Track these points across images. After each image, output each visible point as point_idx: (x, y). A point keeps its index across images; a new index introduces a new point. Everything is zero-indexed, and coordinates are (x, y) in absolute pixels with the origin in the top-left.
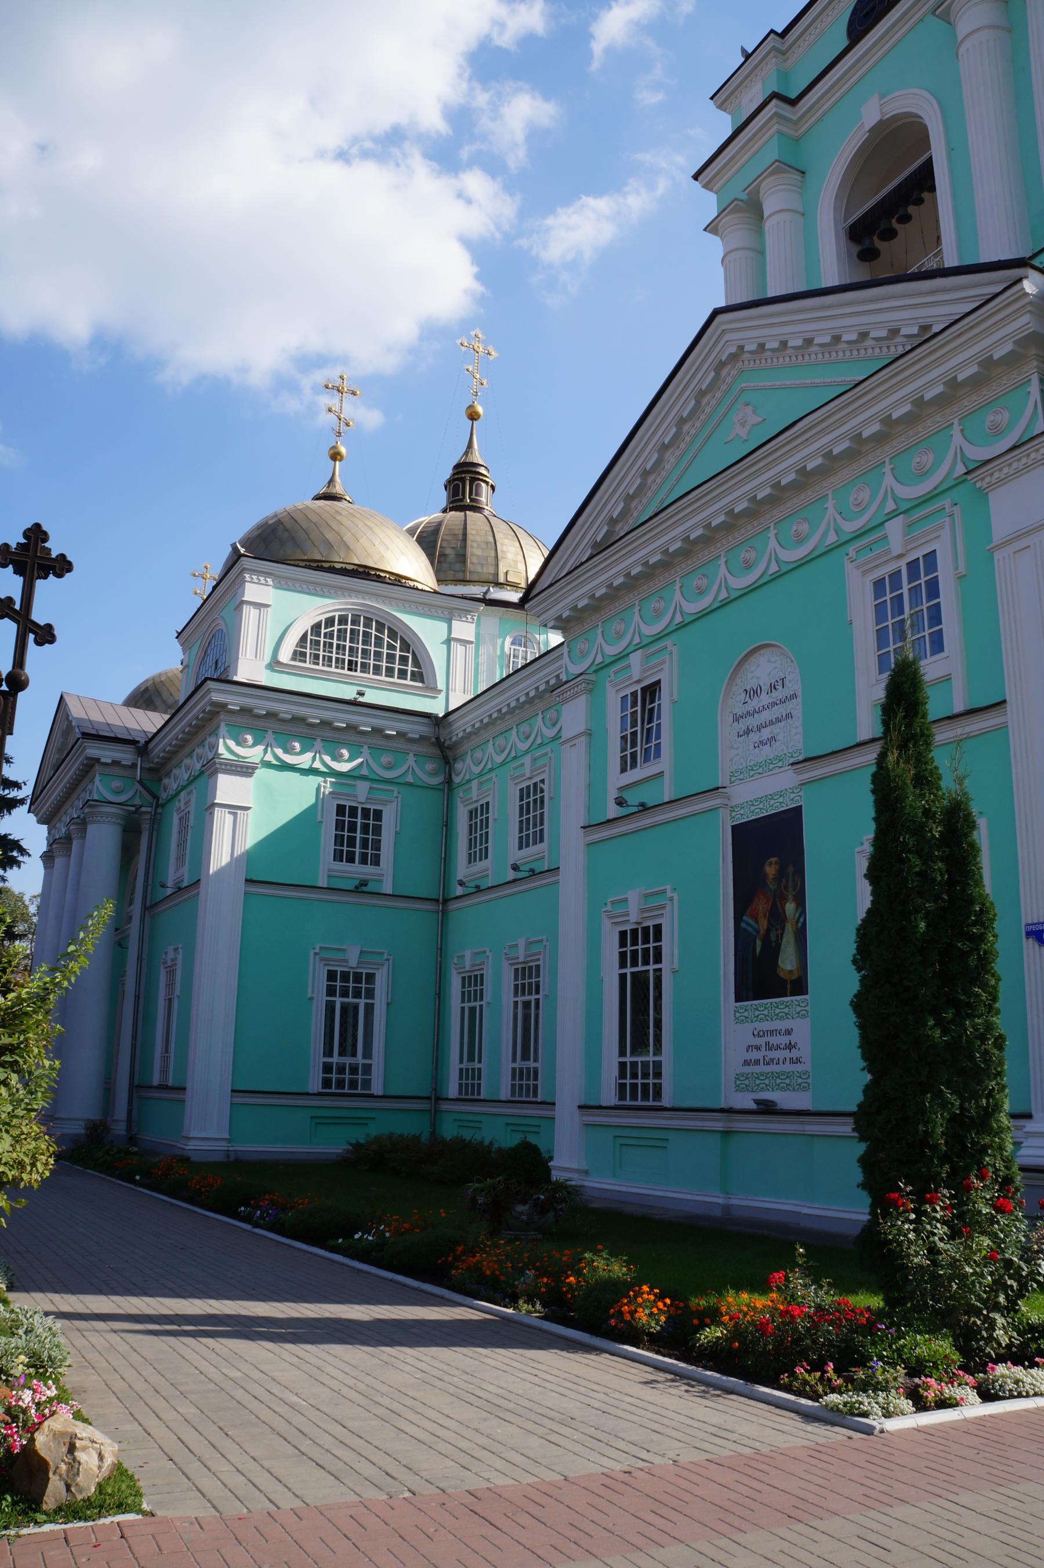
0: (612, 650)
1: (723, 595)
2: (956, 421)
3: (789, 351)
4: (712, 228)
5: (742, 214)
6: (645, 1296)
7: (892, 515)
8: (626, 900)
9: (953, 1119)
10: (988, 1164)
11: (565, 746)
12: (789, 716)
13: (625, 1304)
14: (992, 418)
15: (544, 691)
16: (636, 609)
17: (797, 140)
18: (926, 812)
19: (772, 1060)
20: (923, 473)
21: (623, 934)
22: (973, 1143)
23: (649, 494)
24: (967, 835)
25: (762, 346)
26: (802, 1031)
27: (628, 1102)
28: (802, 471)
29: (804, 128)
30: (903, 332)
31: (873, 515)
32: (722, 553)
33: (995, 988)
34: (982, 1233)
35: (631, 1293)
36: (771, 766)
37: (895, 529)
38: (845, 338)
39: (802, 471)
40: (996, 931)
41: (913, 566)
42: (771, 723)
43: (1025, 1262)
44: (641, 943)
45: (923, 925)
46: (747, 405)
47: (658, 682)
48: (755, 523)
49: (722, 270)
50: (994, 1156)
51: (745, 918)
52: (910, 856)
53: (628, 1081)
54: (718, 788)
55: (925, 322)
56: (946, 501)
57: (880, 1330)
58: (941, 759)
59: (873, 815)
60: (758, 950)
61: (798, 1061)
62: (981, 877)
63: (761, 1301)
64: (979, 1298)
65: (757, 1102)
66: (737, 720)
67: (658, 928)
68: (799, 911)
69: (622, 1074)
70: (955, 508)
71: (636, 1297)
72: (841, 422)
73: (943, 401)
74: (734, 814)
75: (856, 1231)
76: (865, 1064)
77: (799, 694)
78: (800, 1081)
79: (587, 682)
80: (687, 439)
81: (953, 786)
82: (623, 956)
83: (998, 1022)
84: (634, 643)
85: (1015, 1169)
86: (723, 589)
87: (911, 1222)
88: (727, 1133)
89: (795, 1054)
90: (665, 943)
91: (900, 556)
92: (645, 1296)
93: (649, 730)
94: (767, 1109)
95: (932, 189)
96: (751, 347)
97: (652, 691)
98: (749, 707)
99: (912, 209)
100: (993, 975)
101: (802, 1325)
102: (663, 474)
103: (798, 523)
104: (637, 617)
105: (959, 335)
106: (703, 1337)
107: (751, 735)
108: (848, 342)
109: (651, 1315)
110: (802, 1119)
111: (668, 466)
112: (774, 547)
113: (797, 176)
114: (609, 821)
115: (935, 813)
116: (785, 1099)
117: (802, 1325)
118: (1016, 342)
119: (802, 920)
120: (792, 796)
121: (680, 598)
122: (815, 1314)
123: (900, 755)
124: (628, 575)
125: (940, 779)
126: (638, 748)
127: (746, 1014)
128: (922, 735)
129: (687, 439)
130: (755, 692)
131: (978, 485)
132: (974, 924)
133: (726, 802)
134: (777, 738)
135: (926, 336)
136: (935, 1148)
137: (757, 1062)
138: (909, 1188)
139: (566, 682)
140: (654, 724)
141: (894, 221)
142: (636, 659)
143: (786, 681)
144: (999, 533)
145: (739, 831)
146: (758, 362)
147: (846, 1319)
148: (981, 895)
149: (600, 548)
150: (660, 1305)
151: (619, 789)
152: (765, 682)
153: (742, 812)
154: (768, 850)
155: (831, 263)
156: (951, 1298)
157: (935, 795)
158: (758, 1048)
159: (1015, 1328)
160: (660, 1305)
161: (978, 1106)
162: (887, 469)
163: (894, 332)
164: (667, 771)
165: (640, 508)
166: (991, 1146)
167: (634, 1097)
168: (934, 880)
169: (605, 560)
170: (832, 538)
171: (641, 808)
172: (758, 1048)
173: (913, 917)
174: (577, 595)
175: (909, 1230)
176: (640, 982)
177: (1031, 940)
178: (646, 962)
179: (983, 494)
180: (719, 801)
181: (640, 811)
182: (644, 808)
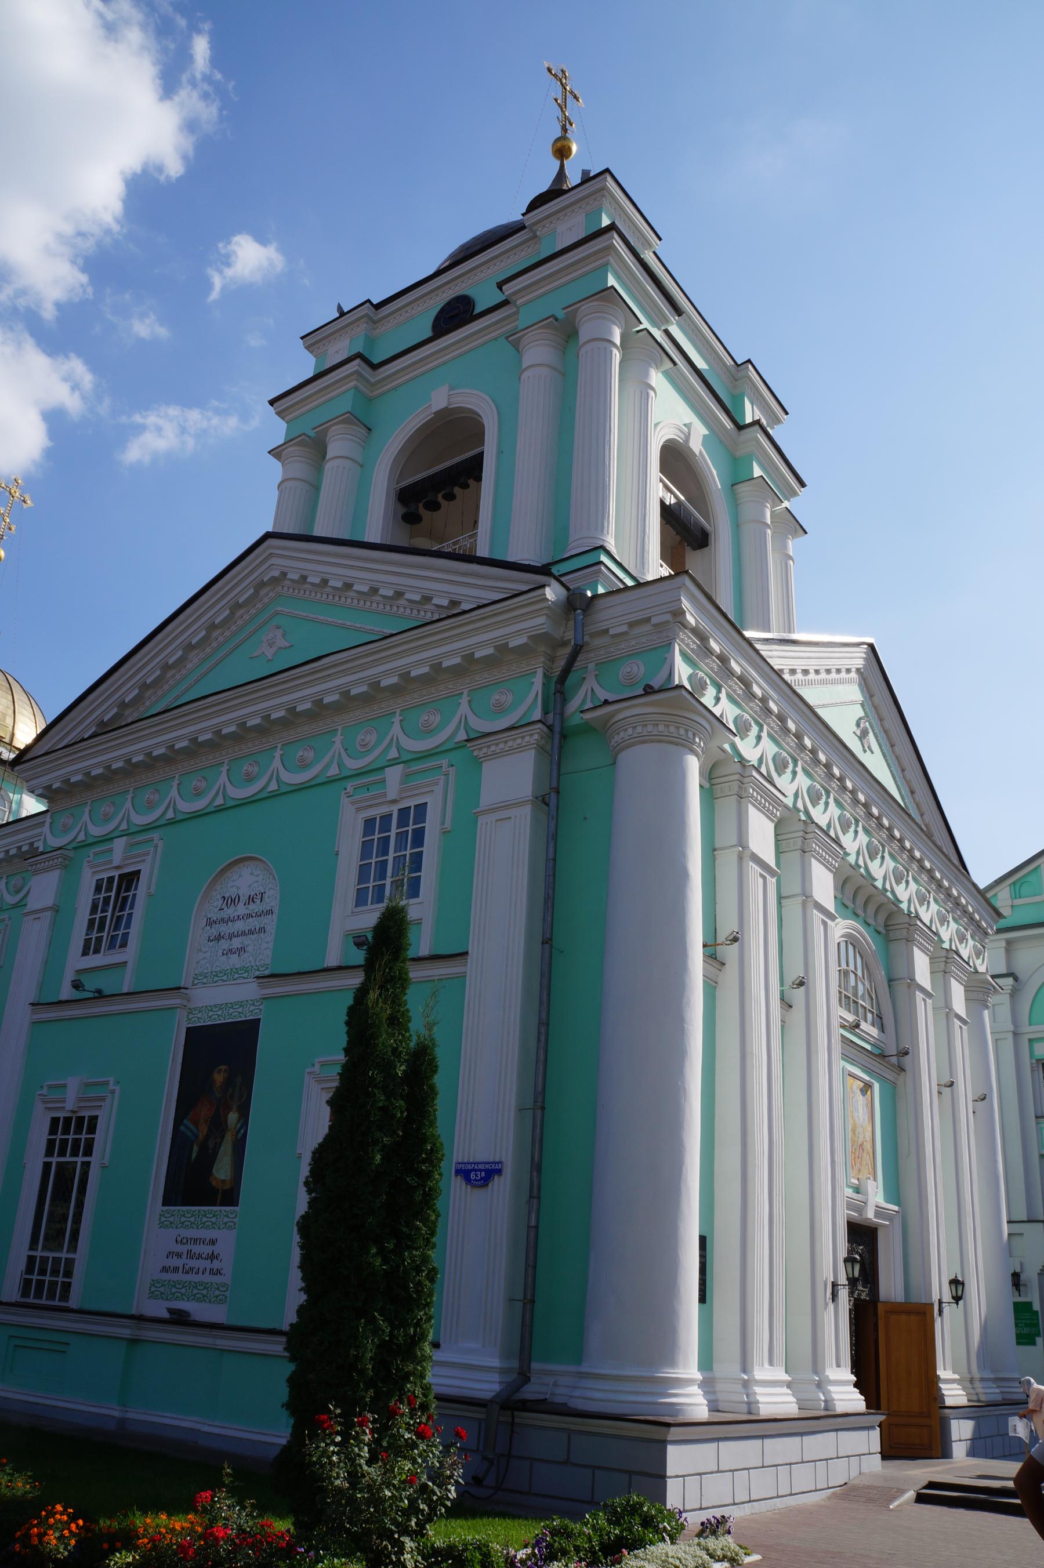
0: (96, 831)
1: (219, 801)
2: (466, 692)
3: (327, 590)
4: (276, 453)
5: (305, 450)
6: (58, 1516)
7: (394, 762)
8: (64, 1086)
9: (382, 1346)
10: (409, 1390)
11: (26, 918)
12: (262, 930)
13: (35, 1526)
14: (498, 697)
15: (14, 856)
16: (130, 796)
17: (370, 400)
18: (395, 1050)
19: (192, 1269)
20: (429, 731)
21: (55, 1121)
22: (398, 1370)
23: (166, 687)
24: (430, 1078)
25: (304, 578)
26: (226, 1242)
27: (31, 1300)
28: (319, 703)
29: (380, 391)
30: (435, 601)
31: (376, 758)
32: (226, 761)
33: (434, 1223)
34: (405, 1458)
35: (44, 1513)
36: (236, 976)
37: (393, 775)
38: (382, 592)
39: (319, 703)
40: (442, 1170)
41: (404, 812)
42: (244, 934)
43: (438, 1486)
44: (72, 1133)
45: (378, 1157)
46: (278, 627)
47: (139, 872)
48: (264, 740)
49: (276, 493)
50: (415, 1383)
51: (185, 1121)
52: (376, 1091)
53: (35, 1277)
54: (179, 988)
55: (457, 598)
56: (444, 761)
57: (298, 1553)
58: (414, 1000)
59: (344, 1044)
60: (194, 1155)
61: (218, 1272)
62: (435, 1118)
63: (179, 1523)
64: (394, 1521)
65: (171, 1311)
66: (211, 925)
67: (94, 1120)
68: (242, 1122)
69: (30, 1269)
70: (451, 769)
71: (47, 1517)
72: (363, 668)
73: (458, 672)
74: (191, 1016)
75: (274, 1453)
76: (303, 1285)
77: (276, 910)
78: (217, 1293)
79: (65, 858)
80: (214, 644)
81: (423, 1031)
82: (51, 1144)
83: (433, 1255)
84: (121, 828)
85: (431, 1397)
86: (221, 795)
87: (336, 1444)
88: (133, 1342)
89: (216, 1264)
90: (98, 1136)
91: (394, 802)
92: (58, 1516)
93: (119, 918)
94: (179, 1319)
95: (479, 479)
96: (293, 576)
97: (130, 879)
98: (225, 914)
99: (457, 490)
100: (434, 1211)
101: (224, 1547)
102: (184, 671)
103: (305, 749)
104: (128, 804)
105: (483, 619)
106: (112, 1563)
107: (222, 941)
108: (383, 597)
109: (58, 1539)
110: (215, 1332)
111: (190, 666)
112: (277, 768)
113: (364, 431)
114: (60, 1002)
115: (401, 1052)
116: (199, 1311)
117: (224, 1547)
118: (529, 637)
119: (242, 1131)
120: (252, 1008)
121: (176, 797)
122: (237, 1536)
123: (380, 994)
124: (128, 761)
125: (409, 1021)
126: (105, 934)
127: (172, 1219)
128: (400, 978)
129: (214, 644)
130: (233, 901)
131: (475, 753)
132: (424, 1162)
133: (185, 1003)
134: (247, 949)
135: (454, 612)
136: (362, 1372)
137: (176, 1270)
138: (338, 1411)
139: (42, 853)
140: (126, 913)
141: (440, 496)
142: (119, 845)
143: (266, 896)
144: (486, 800)
145: (194, 1036)
146: (296, 591)
147: (267, 1543)
148: (433, 1135)
149: (105, 729)
150: (73, 1526)
151: (77, 971)
152: (244, 893)
153: (199, 1015)
154: (220, 1061)
155: (376, 521)
156: (367, 1521)
157: (403, 1036)
158: (179, 1255)
159: (420, 1552)
160: (73, 1526)
161: (406, 1334)
162: (397, 719)
163: (427, 599)
164: (131, 962)
165: (153, 698)
166: (413, 1374)
167: (38, 1295)
168: (393, 1116)
169: (108, 741)
170: (334, 771)
171: (96, 995)
172: (179, 1255)
173: (370, 1149)
174: (74, 769)
175: (333, 1452)
176: (64, 1173)
177: (459, 1178)
178: (75, 1154)
179: (478, 762)
180: (178, 1001)
181: (95, 998)
182: (100, 995)
